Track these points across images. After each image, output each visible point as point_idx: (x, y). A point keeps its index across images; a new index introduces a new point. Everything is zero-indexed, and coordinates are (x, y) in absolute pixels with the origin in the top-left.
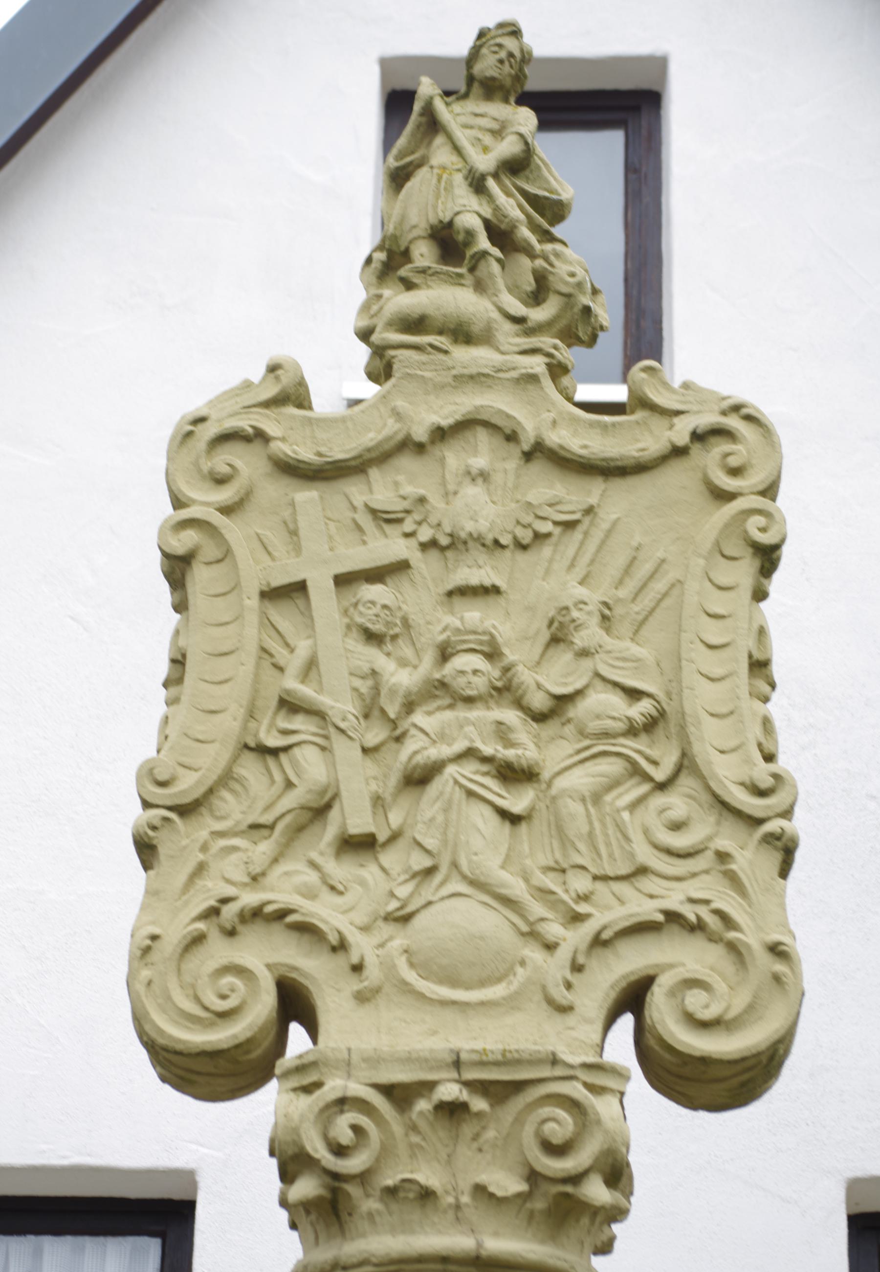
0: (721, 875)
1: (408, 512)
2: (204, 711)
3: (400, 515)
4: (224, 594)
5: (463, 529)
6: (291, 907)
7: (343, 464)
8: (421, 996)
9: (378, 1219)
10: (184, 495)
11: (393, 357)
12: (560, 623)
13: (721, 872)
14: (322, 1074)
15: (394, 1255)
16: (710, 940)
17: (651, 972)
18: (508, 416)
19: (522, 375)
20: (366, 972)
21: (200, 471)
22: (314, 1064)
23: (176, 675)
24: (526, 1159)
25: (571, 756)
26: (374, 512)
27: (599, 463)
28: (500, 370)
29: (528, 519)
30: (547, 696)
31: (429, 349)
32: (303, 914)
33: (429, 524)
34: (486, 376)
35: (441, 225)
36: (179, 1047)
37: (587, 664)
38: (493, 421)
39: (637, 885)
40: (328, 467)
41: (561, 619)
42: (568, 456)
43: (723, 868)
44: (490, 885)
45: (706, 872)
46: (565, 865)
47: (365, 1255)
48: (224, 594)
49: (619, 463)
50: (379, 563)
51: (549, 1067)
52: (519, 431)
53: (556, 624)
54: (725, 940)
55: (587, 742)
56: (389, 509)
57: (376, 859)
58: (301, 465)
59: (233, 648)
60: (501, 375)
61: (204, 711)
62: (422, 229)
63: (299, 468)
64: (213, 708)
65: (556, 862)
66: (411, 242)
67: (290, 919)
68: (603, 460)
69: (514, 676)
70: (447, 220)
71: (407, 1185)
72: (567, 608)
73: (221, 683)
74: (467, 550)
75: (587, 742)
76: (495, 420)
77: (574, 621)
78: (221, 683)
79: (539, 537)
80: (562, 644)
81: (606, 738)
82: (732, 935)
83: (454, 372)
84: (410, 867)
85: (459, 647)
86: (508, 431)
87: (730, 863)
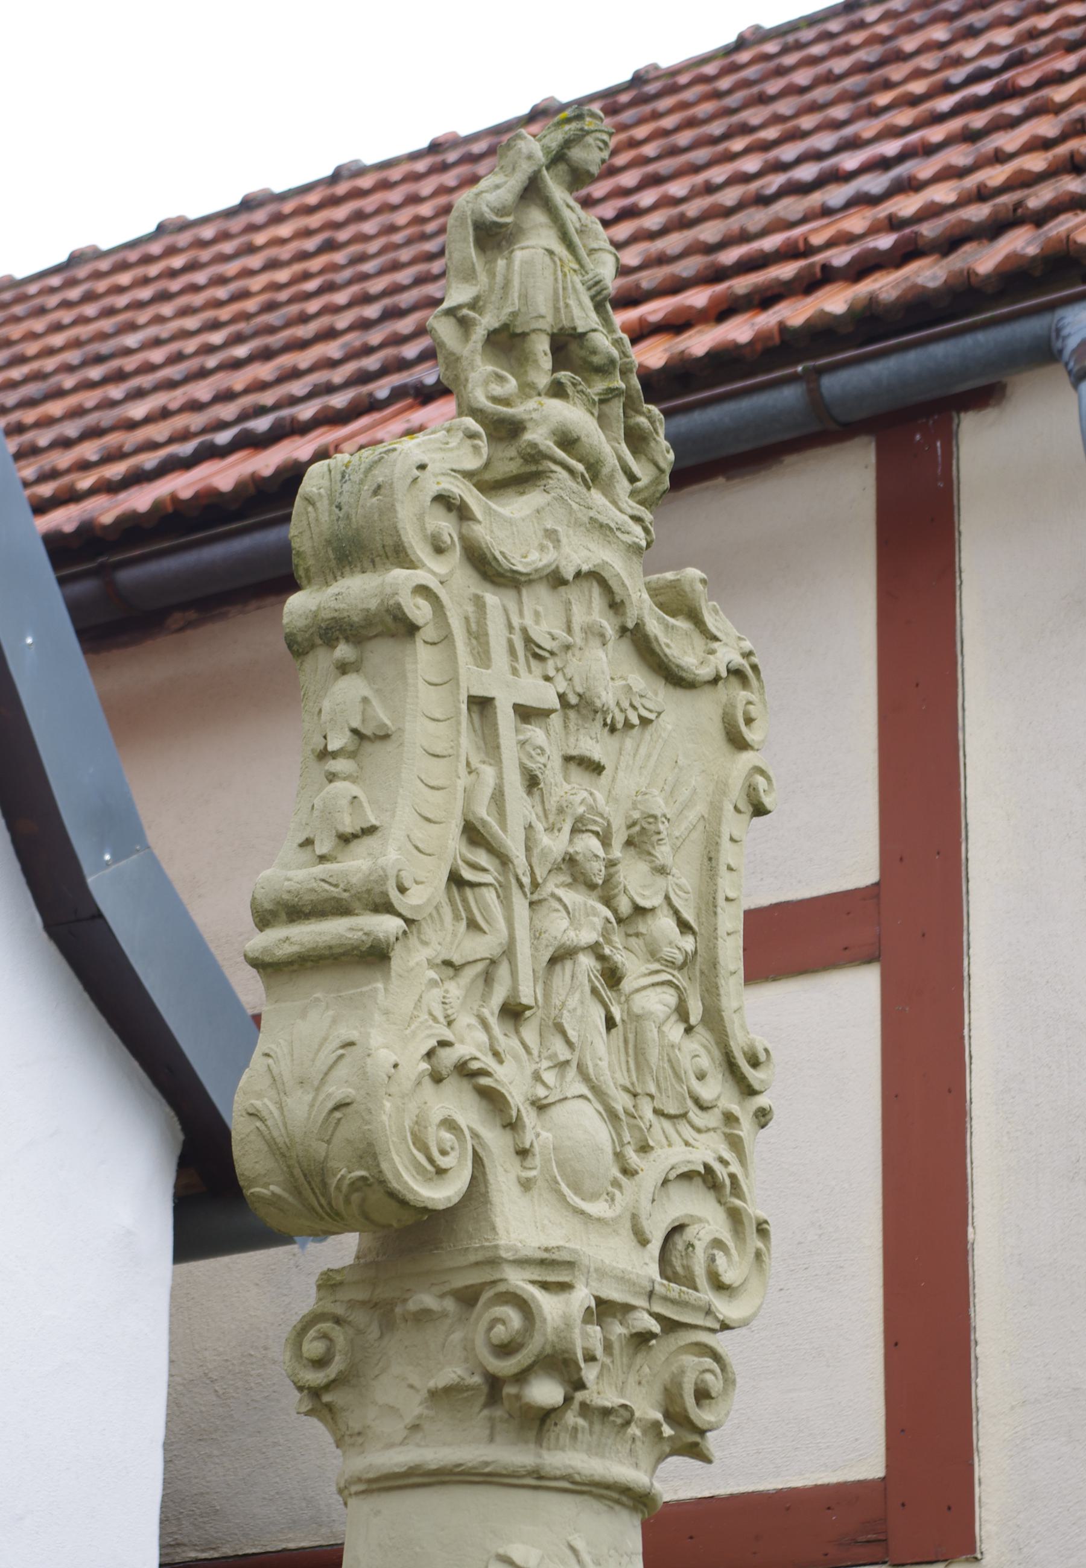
0: (723, 1137)
1: (552, 653)
2: (420, 815)
3: (547, 655)
4: (436, 685)
5: (599, 698)
6: (489, 1070)
7: (518, 576)
8: (562, 1197)
9: (580, 1435)
10: (415, 553)
11: (552, 472)
12: (643, 828)
13: (724, 1134)
14: (574, 1277)
15: (597, 1478)
16: (719, 1202)
17: (686, 1221)
18: (623, 584)
19: (635, 543)
20: (528, 1163)
21: (423, 528)
22: (570, 1265)
23: (351, 748)
24: (485, 1368)
25: (645, 975)
26: (528, 640)
27: (673, 666)
28: (618, 529)
29: (625, 704)
30: (630, 904)
31: (580, 480)
32: (496, 1080)
33: (564, 675)
34: (611, 529)
35: (571, 332)
36: (410, 1197)
37: (661, 881)
38: (610, 583)
39: (679, 1127)
40: (509, 574)
41: (646, 826)
42: (657, 649)
43: (728, 1131)
44: (609, 1096)
45: (714, 1130)
46: (639, 1091)
47: (571, 1471)
48: (436, 685)
49: (684, 675)
50: (542, 706)
51: (702, 1315)
52: (627, 603)
53: (637, 828)
54: (728, 1205)
55: (656, 966)
56: (543, 645)
57: (517, 1032)
58: (494, 563)
59: (445, 753)
60: (618, 534)
61: (420, 815)
62: (546, 324)
63: (490, 564)
64: (429, 816)
65: (633, 1084)
66: (534, 331)
67: (484, 1081)
68: (678, 666)
69: (616, 873)
70: (580, 330)
71: (622, 1411)
72: (655, 817)
73: (432, 788)
74: (594, 720)
75: (656, 966)
76: (613, 583)
77: (659, 833)
78: (432, 788)
79: (628, 725)
80: (632, 848)
81: (671, 968)
82: (738, 1202)
83: (592, 513)
84: (556, 1055)
85: (590, 827)
86: (618, 599)
87: (734, 1128)
